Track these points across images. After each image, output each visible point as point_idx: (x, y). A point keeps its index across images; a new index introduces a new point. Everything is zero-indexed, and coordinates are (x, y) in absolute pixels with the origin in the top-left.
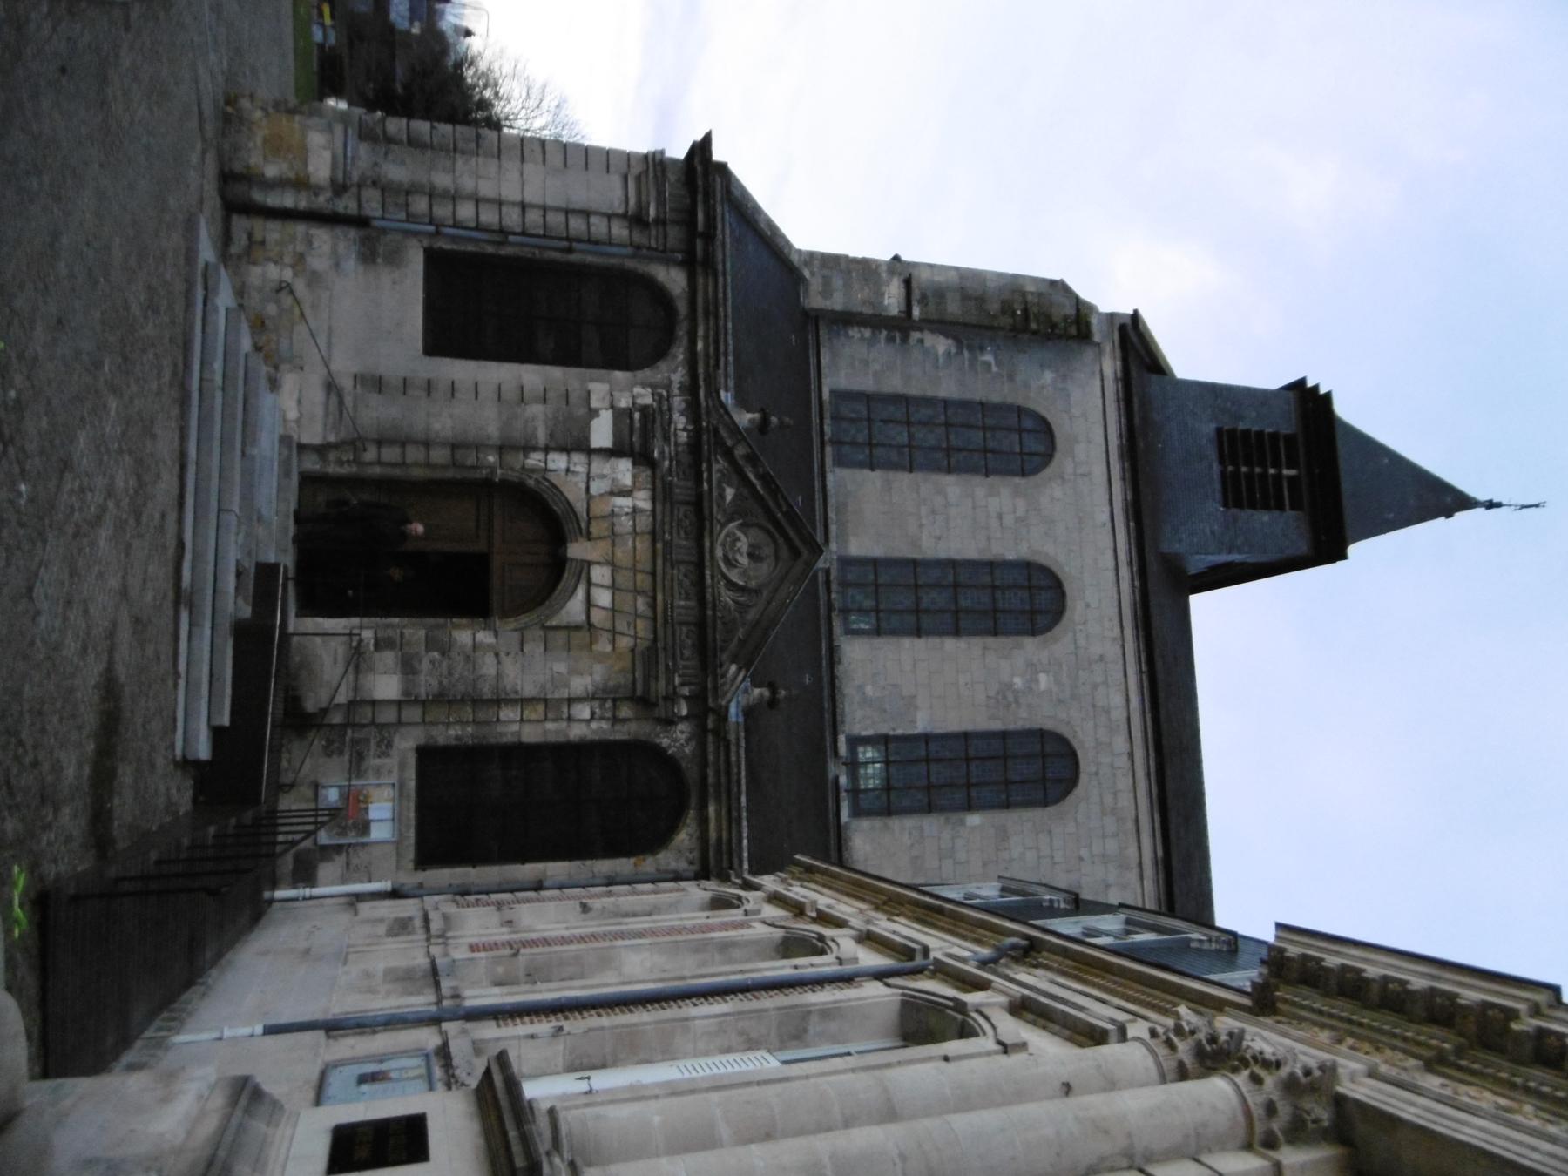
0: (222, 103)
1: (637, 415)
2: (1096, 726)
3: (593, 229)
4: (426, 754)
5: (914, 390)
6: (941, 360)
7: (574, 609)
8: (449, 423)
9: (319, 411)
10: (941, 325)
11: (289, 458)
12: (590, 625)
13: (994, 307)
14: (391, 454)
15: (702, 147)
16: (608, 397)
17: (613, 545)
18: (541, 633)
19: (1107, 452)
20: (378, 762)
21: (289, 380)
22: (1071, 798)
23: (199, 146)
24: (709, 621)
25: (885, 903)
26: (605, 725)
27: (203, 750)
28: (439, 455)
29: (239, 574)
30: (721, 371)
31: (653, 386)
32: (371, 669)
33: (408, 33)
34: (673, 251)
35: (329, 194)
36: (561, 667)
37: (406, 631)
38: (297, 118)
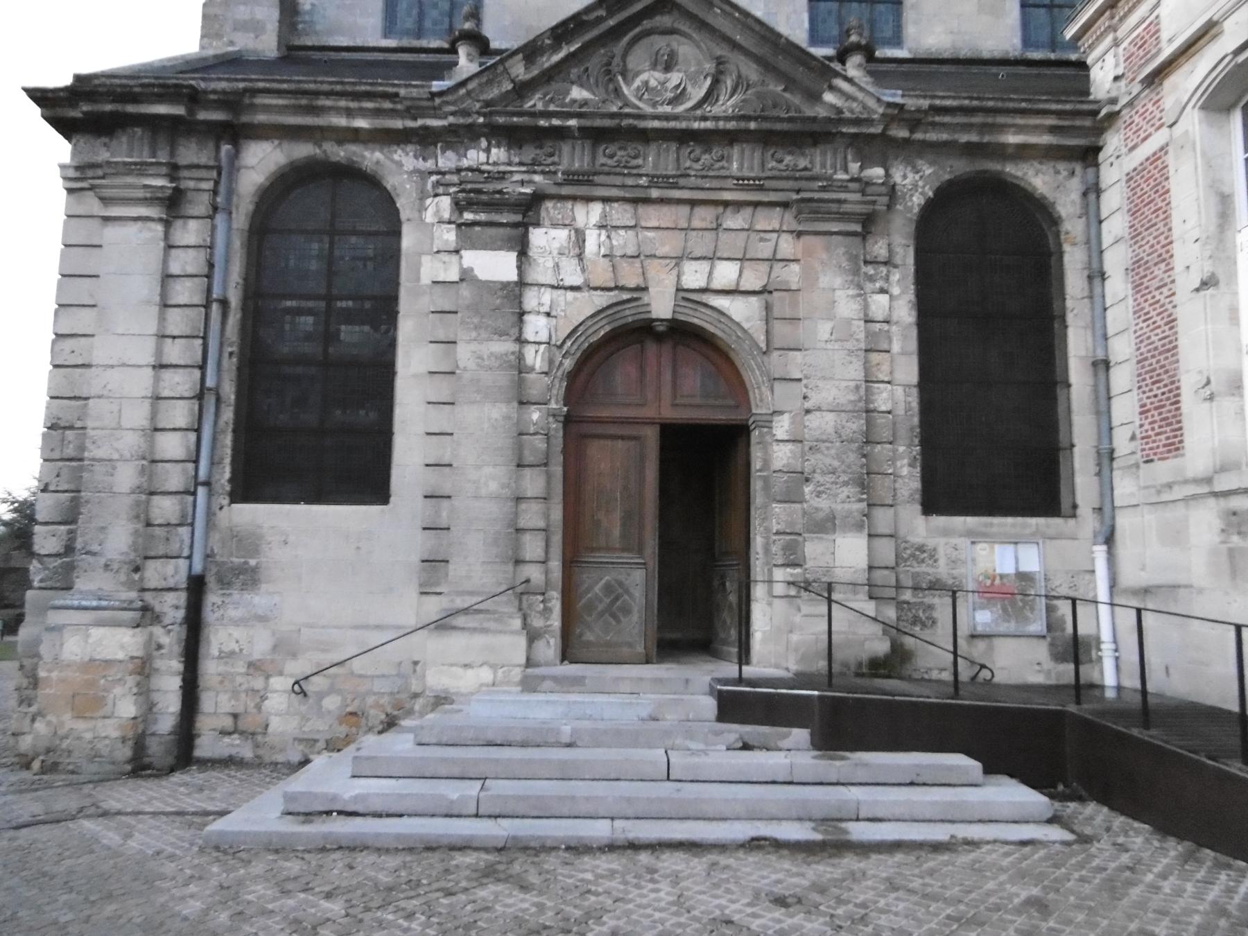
0: (26, 775)
1: (468, 216)
3: (190, 270)
4: (933, 503)
7: (743, 311)
8: (488, 470)
9: (479, 640)
16: (436, 254)
20: (942, 562)
21: (437, 679)
28: (533, 483)
29: (746, 747)
31: (423, 196)
35: (157, 630)
36: (824, 329)
38: (42, 674)
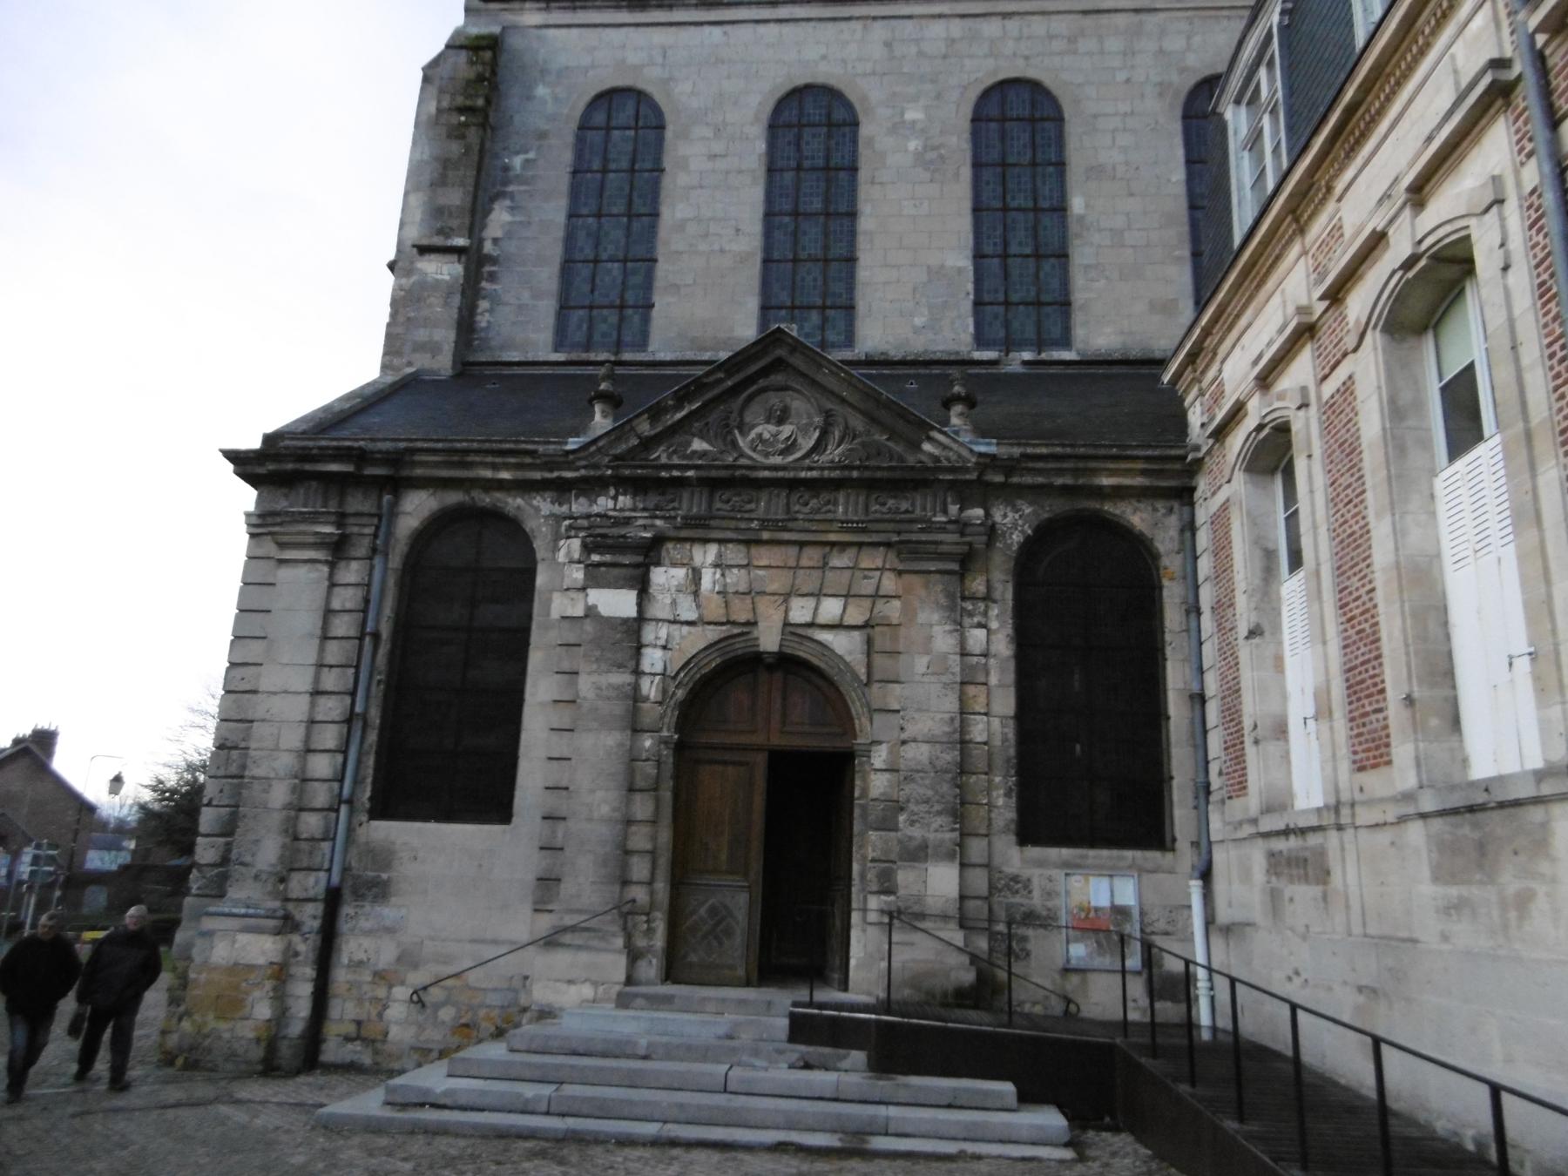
0: (170, 1071)
1: (595, 558)
2: (971, 56)
3: (348, 606)
5: (556, 252)
6: (518, 219)
7: (845, 645)
8: (600, 794)
9: (584, 957)
10: (477, 214)
11: (647, 997)
12: (866, 626)
13: (456, 148)
14: (639, 868)
15: (242, 462)
16: (569, 594)
17: (764, 593)
18: (875, 686)
19: (637, 25)
20: (1036, 894)
21: (541, 994)
22: (1056, 91)
23: (224, 1109)
24: (867, 474)
25: (1297, 220)
26: (994, 611)
27: (1051, 1119)
28: (642, 807)
29: (807, 1066)
30: (541, 449)
31: (557, 537)
32: (920, 899)
33: (134, 852)
34: (380, 506)
36: (921, 663)
37: (871, 855)
38: (192, 975)
